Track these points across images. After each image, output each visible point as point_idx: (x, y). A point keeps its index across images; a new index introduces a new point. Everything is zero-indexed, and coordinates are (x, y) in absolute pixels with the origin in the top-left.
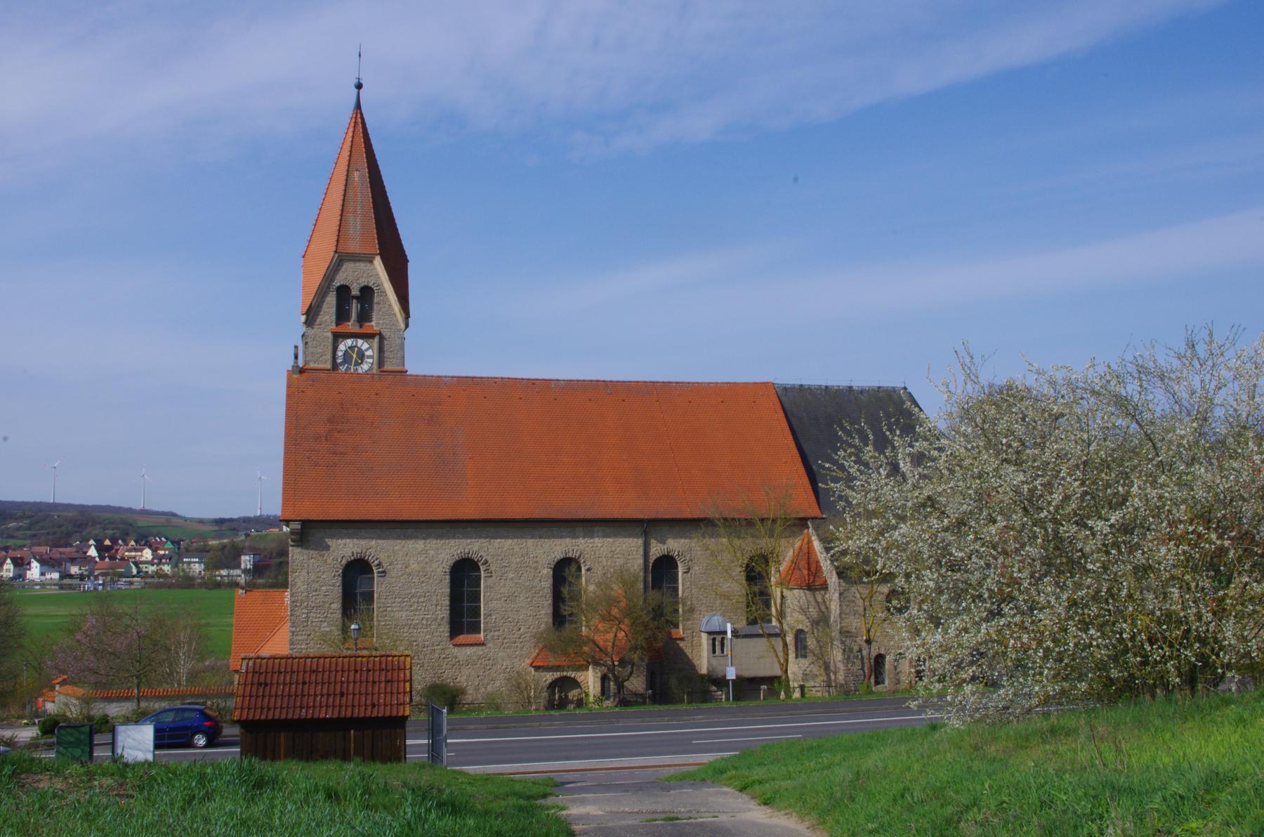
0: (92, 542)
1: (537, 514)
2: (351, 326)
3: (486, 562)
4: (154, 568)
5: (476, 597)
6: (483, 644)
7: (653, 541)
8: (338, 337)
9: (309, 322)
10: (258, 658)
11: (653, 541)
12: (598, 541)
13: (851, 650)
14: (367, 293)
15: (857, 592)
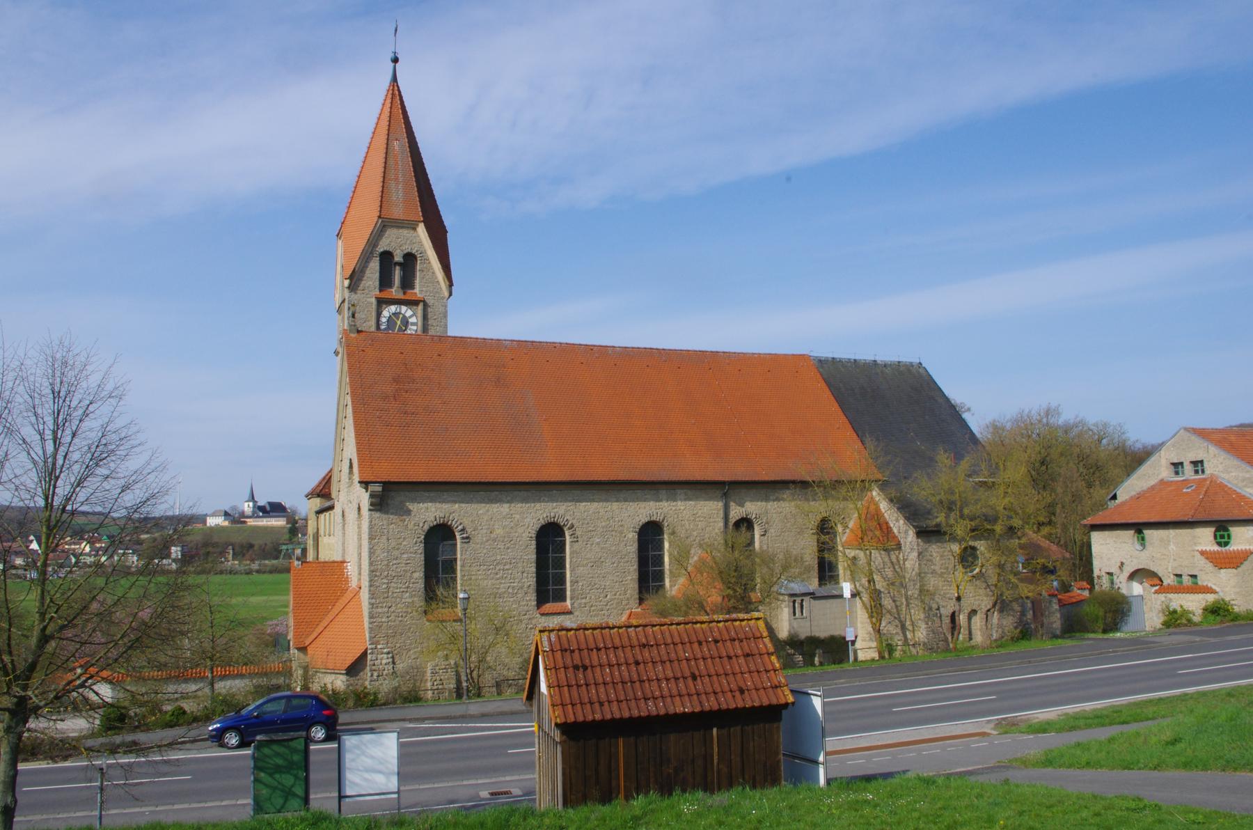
0: (32, 537)
1: (623, 476)
2: (395, 292)
3: (572, 526)
4: (92, 559)
5: (561, 564)
6: (570, 613)
7: (732, 504)
8: (382, 303)
9: (353, 287)
10: (562, 629)
11: (732, 504)
12: (680, 505)
13: (931, 609)
14: (410, 259)
15: (935, 550)
